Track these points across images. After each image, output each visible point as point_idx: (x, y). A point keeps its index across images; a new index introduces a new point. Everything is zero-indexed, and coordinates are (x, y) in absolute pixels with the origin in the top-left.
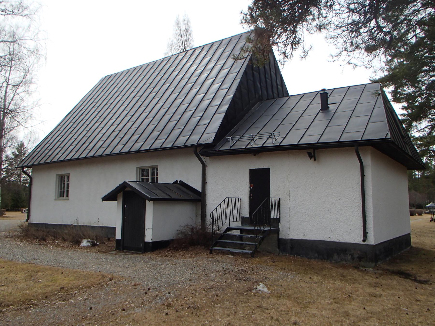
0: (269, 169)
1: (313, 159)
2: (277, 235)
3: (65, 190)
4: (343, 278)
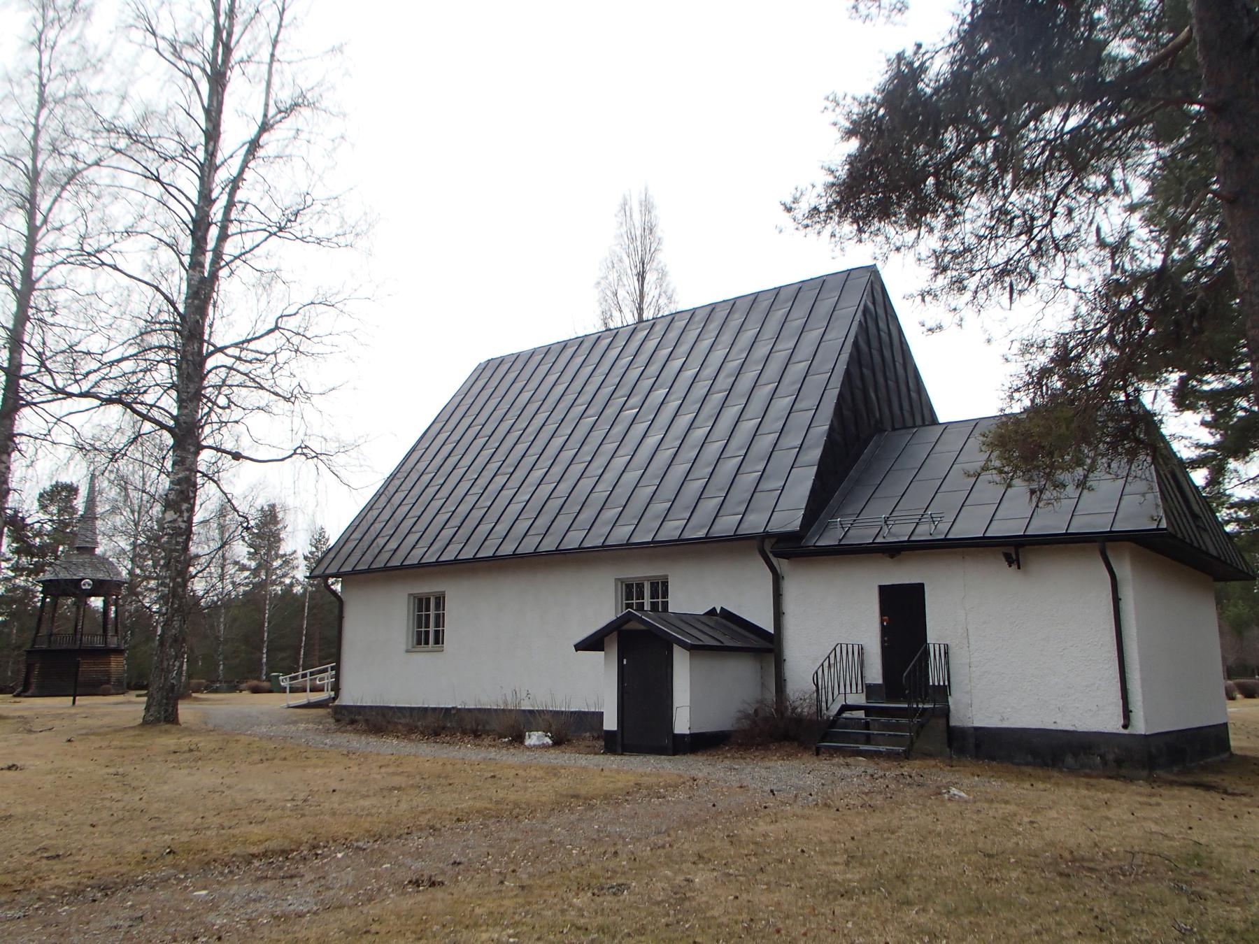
0: (922, 585)
1: (1014, 567)
2: (944, 720)
3: (432, 629)
4: (1089, 786)
